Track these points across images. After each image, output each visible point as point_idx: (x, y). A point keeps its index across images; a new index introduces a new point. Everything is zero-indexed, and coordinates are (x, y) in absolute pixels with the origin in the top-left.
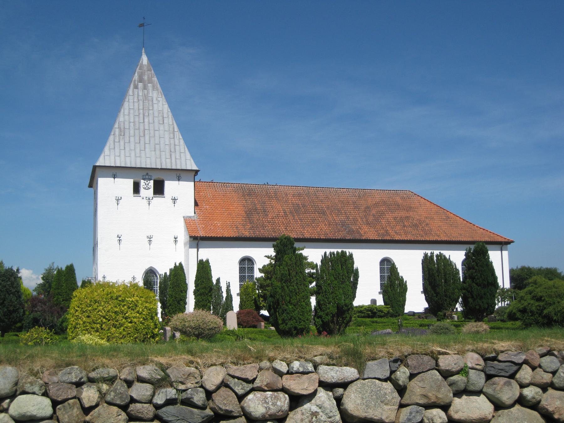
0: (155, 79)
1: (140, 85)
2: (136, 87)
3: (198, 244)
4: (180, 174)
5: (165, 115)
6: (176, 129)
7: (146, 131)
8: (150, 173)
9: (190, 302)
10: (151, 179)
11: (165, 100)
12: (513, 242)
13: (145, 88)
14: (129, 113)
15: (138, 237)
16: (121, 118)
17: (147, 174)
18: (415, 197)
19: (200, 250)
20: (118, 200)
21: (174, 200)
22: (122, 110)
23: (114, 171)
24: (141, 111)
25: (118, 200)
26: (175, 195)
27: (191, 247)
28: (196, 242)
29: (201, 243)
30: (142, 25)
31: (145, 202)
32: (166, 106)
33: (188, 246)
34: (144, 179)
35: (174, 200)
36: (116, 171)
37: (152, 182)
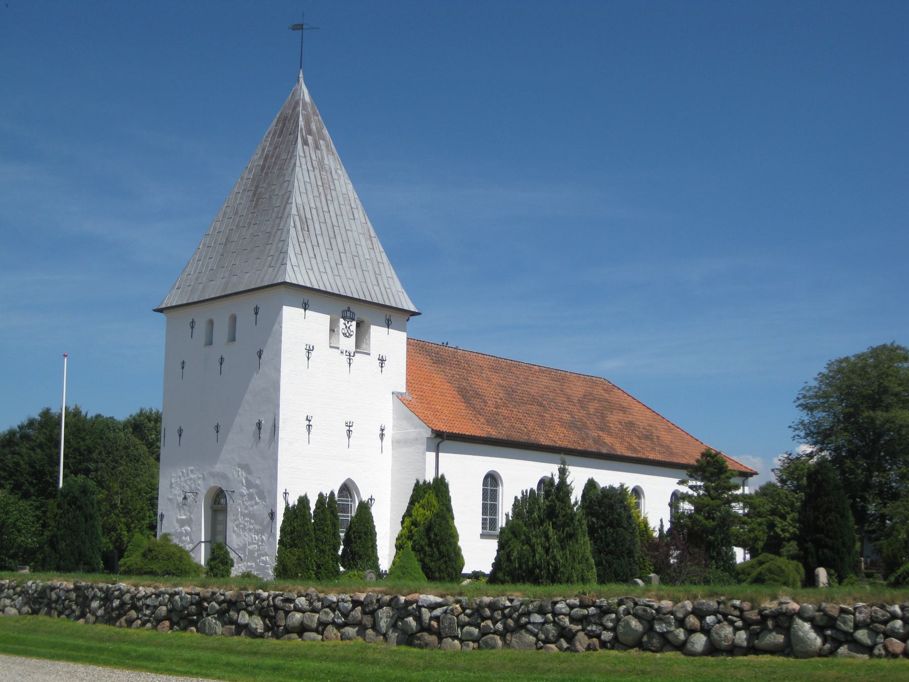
0: (326, 132)
1: (310, 138)
2: (305, 143)
3: (438, 445)
4: (392, 316)
5: (353, 205)
6: (373, 234)
7: (336, 228)
8: (355, 308)
9: (388, 544)
10: (353, 319)
11: (346, 176)
12: (756, 474)
13: (317, 147)
14: (306, 190)
15: (341, 422)
16: (297, 198)
17: (349, 310)
18: (616, 390)
19: (440, 454)
20: (309, 350)
21: (382, 361)
22: (296, 184)
23: (306, 296)
24: (321, 189)
25: (309, 350)
26: (383, 353)
27: (429, 450)
28: (439, 440)
29: (447, 443)
30: (299, 27)
31: (345, 358)
32: (350, 186)
33: (425, 447)
34: (344, 318)
35: (382, 361)
36: (310, 297)
37: (354, 323)
